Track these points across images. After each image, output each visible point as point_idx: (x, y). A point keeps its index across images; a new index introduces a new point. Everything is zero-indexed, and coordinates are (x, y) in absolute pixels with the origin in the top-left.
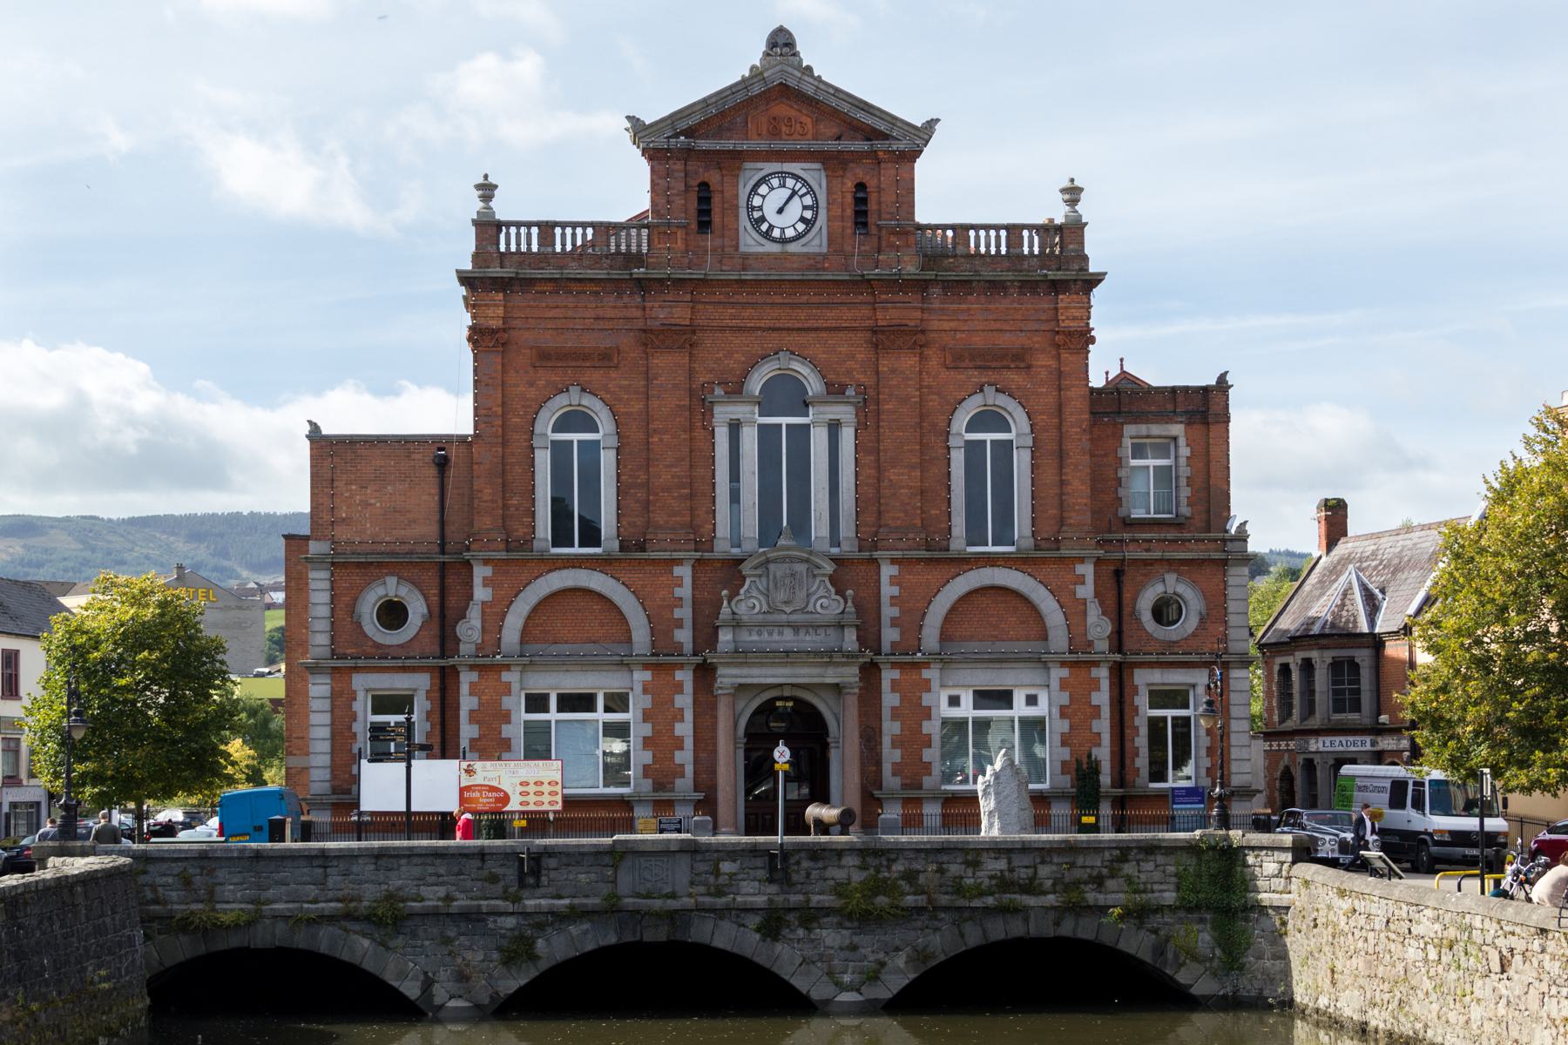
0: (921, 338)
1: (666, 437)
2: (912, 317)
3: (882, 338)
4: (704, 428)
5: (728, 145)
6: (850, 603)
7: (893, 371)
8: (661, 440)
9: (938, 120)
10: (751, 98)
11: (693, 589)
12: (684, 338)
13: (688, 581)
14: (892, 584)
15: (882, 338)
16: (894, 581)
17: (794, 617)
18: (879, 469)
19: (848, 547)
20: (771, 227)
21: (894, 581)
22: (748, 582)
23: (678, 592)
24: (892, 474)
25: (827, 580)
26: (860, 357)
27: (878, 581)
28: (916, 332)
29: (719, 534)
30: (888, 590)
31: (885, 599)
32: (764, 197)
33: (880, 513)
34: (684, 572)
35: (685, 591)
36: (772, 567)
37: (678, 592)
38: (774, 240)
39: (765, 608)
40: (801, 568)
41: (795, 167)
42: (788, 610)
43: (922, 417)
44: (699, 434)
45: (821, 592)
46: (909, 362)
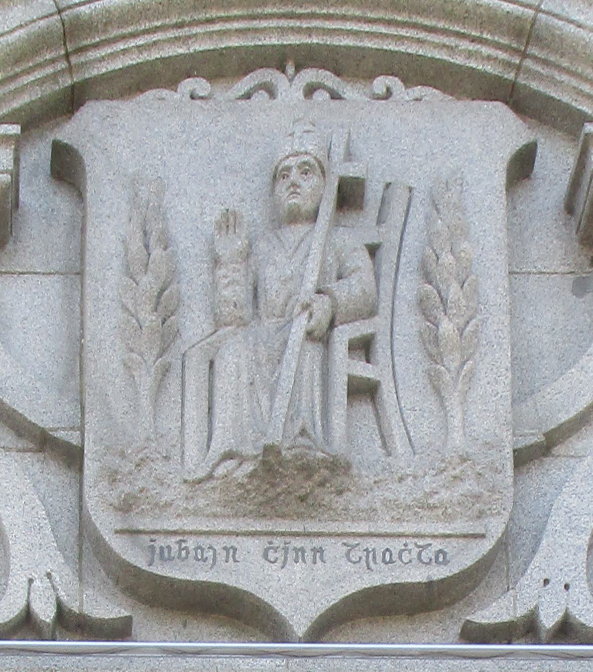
42: (298, 584)
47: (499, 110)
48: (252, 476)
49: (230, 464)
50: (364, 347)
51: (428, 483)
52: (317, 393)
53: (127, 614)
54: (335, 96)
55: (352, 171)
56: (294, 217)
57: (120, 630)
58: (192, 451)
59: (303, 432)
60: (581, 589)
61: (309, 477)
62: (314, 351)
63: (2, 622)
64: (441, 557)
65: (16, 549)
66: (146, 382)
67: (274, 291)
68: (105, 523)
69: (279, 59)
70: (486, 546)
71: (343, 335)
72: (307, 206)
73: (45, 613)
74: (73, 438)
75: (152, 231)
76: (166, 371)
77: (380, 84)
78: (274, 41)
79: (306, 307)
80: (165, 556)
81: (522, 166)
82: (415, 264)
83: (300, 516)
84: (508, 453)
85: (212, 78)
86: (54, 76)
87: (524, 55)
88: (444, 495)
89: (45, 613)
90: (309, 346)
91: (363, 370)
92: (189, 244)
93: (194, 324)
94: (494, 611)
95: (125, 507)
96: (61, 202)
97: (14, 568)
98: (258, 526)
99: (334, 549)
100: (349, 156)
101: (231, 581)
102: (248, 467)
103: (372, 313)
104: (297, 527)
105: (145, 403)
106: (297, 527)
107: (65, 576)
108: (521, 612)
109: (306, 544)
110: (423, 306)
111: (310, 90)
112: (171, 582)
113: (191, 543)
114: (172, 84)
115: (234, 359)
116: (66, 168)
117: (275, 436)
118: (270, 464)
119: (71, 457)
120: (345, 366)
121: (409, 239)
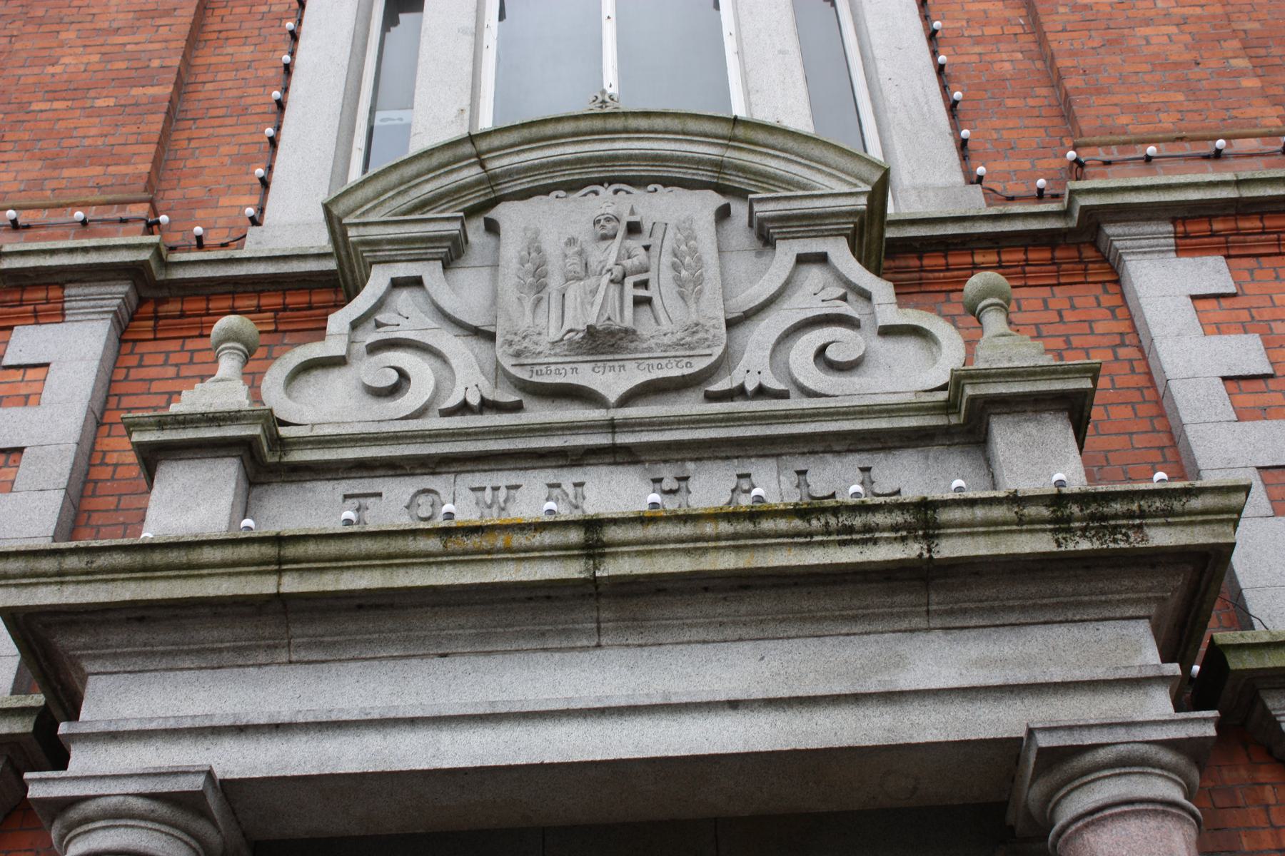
25: (839, 252)
42: (612, 381)
47: (710, 192)
48: (583, 338)
49: (571, 334)
50: (644, 284)
51: (679, 335)
52: (617, 304)
53: (518, 399)
54: (628, 193)
55: (633, 219)
56: (604, 238)
58: (552, 330)
59: (609, 319)
62: (614, 289)
63: (1282, 422)
64: (689, 365)
67: (594, 265)
68: (507, 363)
69: (601, 182)
70: (713, 359)
71: (629, 281)
72: (611, 233)
74: (492, 329)
76: (539, 300)
77: (651, 187)
78: (596, 175)
79: (609, 270)
81: (723, 214)
82: (670, 250)
83: (612, 353)
84: (723, 321)
85: (566, 191)
86: (485, 195)
88: (688, 339)
90: (612, 286)
91: (641, 292)
93: (555, 282)
96: (489, 240)
97: (458, 382)
98: (589, 358)
100: (632, 212)
101: (575, 382)
102: (581, 335)
103: (647, 271)
104: (610, 357)
106: (610, 357)
108: (735, 385)
109: (616, 364)
110: (675, 267)
111: (616, 192)
112: (543, 384)
113: (553, 367)
114: (547, 193)
115: (574, 291)
116: (492, 228)
117: (592, 321)
118: (591, 332)
119: (491, 337)
121: (666, 243)
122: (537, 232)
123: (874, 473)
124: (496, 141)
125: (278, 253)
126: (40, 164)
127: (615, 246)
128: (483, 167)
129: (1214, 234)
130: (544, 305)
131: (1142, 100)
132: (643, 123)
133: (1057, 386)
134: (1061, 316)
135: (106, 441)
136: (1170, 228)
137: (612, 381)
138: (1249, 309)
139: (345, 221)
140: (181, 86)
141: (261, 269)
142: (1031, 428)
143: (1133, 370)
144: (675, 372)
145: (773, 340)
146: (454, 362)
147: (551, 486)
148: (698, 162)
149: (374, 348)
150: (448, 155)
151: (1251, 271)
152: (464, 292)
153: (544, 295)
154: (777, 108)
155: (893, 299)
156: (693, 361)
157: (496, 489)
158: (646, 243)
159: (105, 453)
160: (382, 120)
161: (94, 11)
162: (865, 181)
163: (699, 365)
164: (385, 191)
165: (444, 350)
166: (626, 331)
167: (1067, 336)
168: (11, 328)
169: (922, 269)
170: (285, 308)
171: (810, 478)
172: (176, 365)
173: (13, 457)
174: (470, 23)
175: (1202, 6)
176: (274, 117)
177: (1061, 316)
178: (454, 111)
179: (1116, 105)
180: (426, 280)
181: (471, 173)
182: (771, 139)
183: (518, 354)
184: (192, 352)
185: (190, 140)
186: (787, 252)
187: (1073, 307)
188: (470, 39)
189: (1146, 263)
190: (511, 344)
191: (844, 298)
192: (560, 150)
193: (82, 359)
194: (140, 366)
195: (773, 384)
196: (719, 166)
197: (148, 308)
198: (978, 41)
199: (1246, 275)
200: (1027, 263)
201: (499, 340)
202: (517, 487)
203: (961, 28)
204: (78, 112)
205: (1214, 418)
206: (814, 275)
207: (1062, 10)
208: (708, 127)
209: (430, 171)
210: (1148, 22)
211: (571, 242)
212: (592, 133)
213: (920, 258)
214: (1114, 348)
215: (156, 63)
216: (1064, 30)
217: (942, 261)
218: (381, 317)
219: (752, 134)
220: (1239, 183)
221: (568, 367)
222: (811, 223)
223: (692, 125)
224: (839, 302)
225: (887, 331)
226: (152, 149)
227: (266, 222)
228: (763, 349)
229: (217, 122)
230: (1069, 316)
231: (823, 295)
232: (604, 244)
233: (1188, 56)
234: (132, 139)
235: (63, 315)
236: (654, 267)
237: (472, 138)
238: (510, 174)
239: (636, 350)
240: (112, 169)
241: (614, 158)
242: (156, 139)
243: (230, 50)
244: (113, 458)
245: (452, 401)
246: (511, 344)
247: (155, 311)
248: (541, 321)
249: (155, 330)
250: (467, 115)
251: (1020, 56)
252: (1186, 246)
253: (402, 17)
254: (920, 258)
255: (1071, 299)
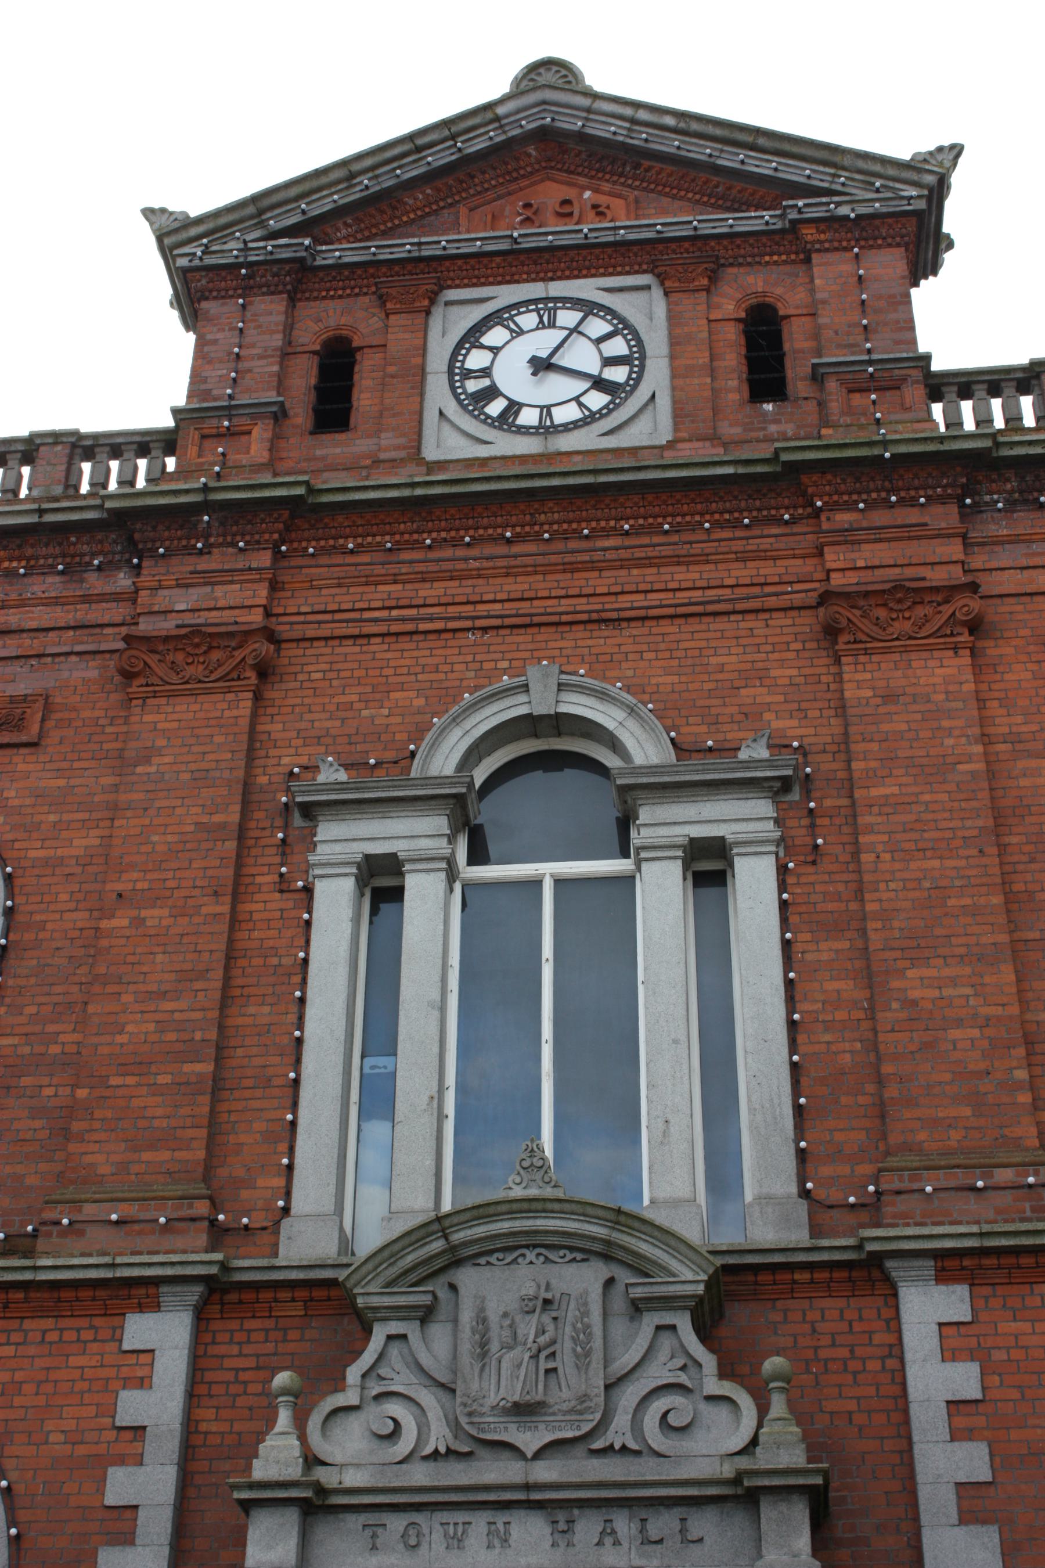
0: (967, 605)
1: (155, 916)
2: (937, 560)
3: (841, 622)
4: (283, 885)
5: (403, 247)
6: (778, 1406)
7: (890, 697)
8: (138, 922)
9: (957, 150)
10: (466, 160)
11: (192, 1396)
12: (255, 661)
13: (172, 1368)
14: (949, 1354)
15: (841, 622)
16: (955, 1343)
17: (545, 1472)
18: (869, 977)
19: (767, 1212)
20: (514, 407)
21: (955, 1343)
22: (379, 1334)
23: (132, 1405)
24: (915, 983)
25: (684, 1322)
26: (782, 674)
27: (896, 1350)
28: (950, 591)
29: (298, 1205)
30: (935, 1382)
31: (927, 1419)
32: (495, 350)
33: (881, 1112)
34: (164, 1334)
35: (158, 1405)
36: (467, 1278)
37: (132, 1405)
38: (524, 431)
39: (439, 1437)
40: (582, 1280)
41: (586, 288)
42: (530, 1440)
43: (1000, 821)
44: (265, 903)
45: (659, 1373)
46: (942, 673)
51: (573, 1403)
57: (469, 1454)
60: (629, 1435)
61: (528, 221)
64: (579, 1428)
65: (433, 1427)
66: (477, 1370)
70: (595, 1423)
71: (543, 1355)
73: (442, 1450)
74: (453, 1386)
75: (482, 1319)
76: (484, 1366)
80: (483, 1431)
84: (602, 1383)
87: (629, 129)
89: (442, 1450)
91: (551, 1365)
92: (493, 1316)
93: (494, 1347)
94: (598, 1445)
95: (470, 1414)
99: (542, 1426)
105: (476, 1375)
107: (449, 1436)
116: (453, 1288)
118: (516, 1404)
120: (543, 1365)
122: (483, 1299)
123: (689, 1522)
124: (455, 1220)
125: (305, 1263)
126: (123, 1145)
127: (534, 1318)
128: (447, 1239)
129: (963, 1268)
130: (487, 1369)
131: (940, 1115)
132: (556, 1206)
133: (801, 1481)
134: (851, 1326)
135: (198, 1411)
136: (932, 1263)
137: (530, 1440)
138: (978, 1336)
139: (355, 1291)
140: (221, 1053)
141: (294, 1275)
142: (783, 1507)
143: (893, 1380)
144: (570, 1434)
145: (634, 1405)
146: (430, 1415)
147: (489, 1523)
148: (593, 1239)
149: (379, 1397)
150: (423, 1232)
151: (987, 1298)
152: (434, 1347)
153: (486, 1360)
154: (666, 1106)
155: (715, 1372)
156: (582, 1425)
157: (456, 1524)
158: (554, 1314)
159: (197, 1422)
160: (372, 1067)
161: (145, 969)
162: (704, 1272)
163: (586, 1428)
164: (381, 1264)
165: (423, 1404)
166: (539, 1403)
167: (852, 1346)
168: (124, 1314)
169: (756, 1283)
170: (312, 1300)
171: (649, 1526)
172: (239, 1343)
173: (139, 1433)
174: (436, 995)
175: (1003, 1005)
176: (291, 1090)
177: (851, 1326)
178: (425, 1099)
179: (919, 1119)
180: (410, 1336)
181: (437, 1245)
182: (643, 1228)
183: (470, 1414)
184: (249, 1331)
185: (230, 1112)
186: (651, 1320)
187: (861, 1319)
188: (436, 1014)
189: (913, 1290)
190: (465, 1405)
191: (683, 1368)
192: (499, 1225)
193: (176, 1348)
194: (214, 1343)
195: (633, 1445)
196: (608, 1243)
197: (216, 1297)
198: (828, 1026)
199: (981, 1303)
200: (831, 1280)
201: (458, 1393)
202: (470, 1523)
203: (816, 1012)
204: (144, 1090)
205: (935, 1439)
206: (667, 1342)
207: (895, 1005)
208: (601, 1213)
209: (410, 1245)
210: (959, 1023)
211: (505, 1315)
212: (521, 1212)
213: (756, 1275)
214: (883, 1359)
215: (198, 1035)
216: (893, 1031)
217: (771, 1277)
218: (382, 1371)
219: (630, 1222)
220: (981, 1235)
221: (502, 1426)
222: (667, 1302)
223: (590, 1210)
224: (680, 1373)
225: (710, 1398)
226: (203, 1133)
227: (293, 1212)
228: (627, 1413)
229: (248, 1094)
230: (857, 1327)
231: (670, 1366)
232: (528, 1317)
233: (982, 1066)
234: (189, 1122)
235: (159, 1306)
236: (559, 1341)
237: (438, 1219)
238: (466, 1244)
239: (545, 1414)
240: (177, 1154)
241: (536, 1232)
242: (205, 1122)
243: (252, 1010)
244: (203, 1427)
245: (428, 1450)
246: (465, 1405)
247: (221, 1299)
248: (485, 1385)
249: (222, 1312)
250: (436, 1101)
251: (858, 1045)
252: (943, 1277)
253: (382, 906)
254: (756, 1275)
255: (860, 1310)
